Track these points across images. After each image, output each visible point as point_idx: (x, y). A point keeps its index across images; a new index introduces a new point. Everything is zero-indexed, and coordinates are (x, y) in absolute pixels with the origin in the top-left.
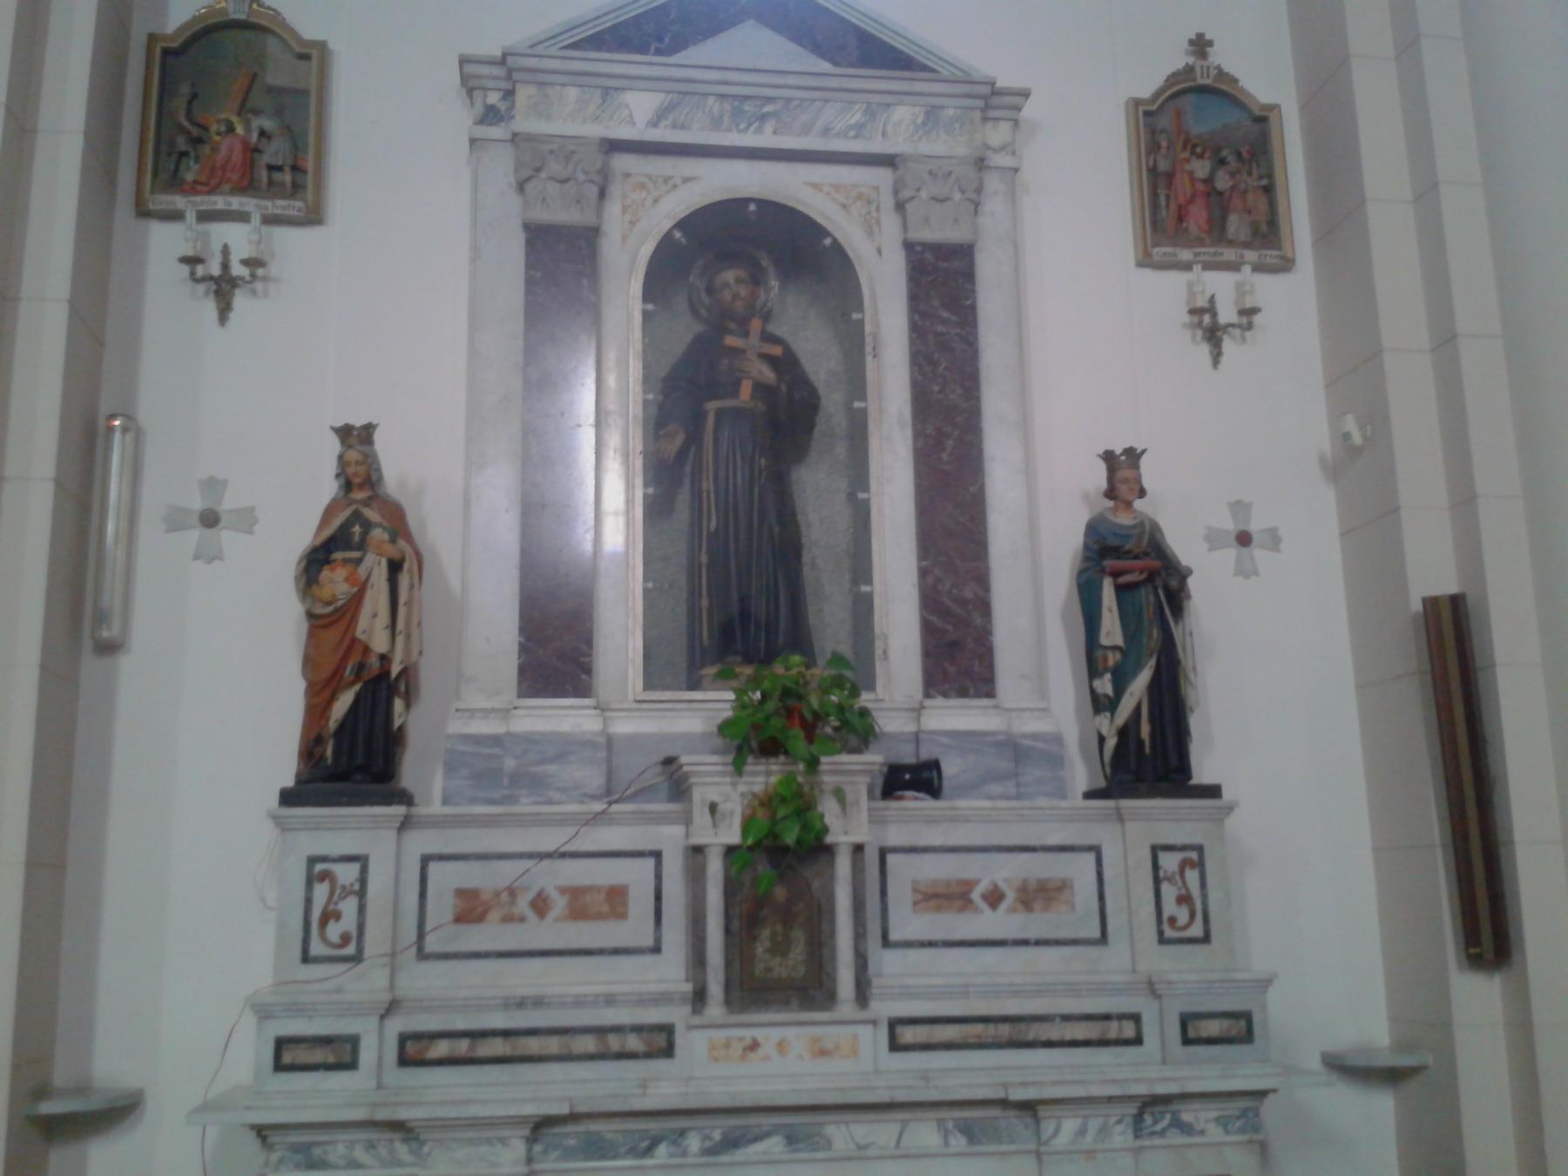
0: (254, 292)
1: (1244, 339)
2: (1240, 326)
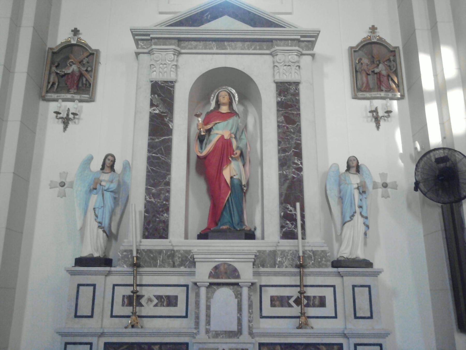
0: (75, 123)
1: (388, 121)
2: (386, 117)
